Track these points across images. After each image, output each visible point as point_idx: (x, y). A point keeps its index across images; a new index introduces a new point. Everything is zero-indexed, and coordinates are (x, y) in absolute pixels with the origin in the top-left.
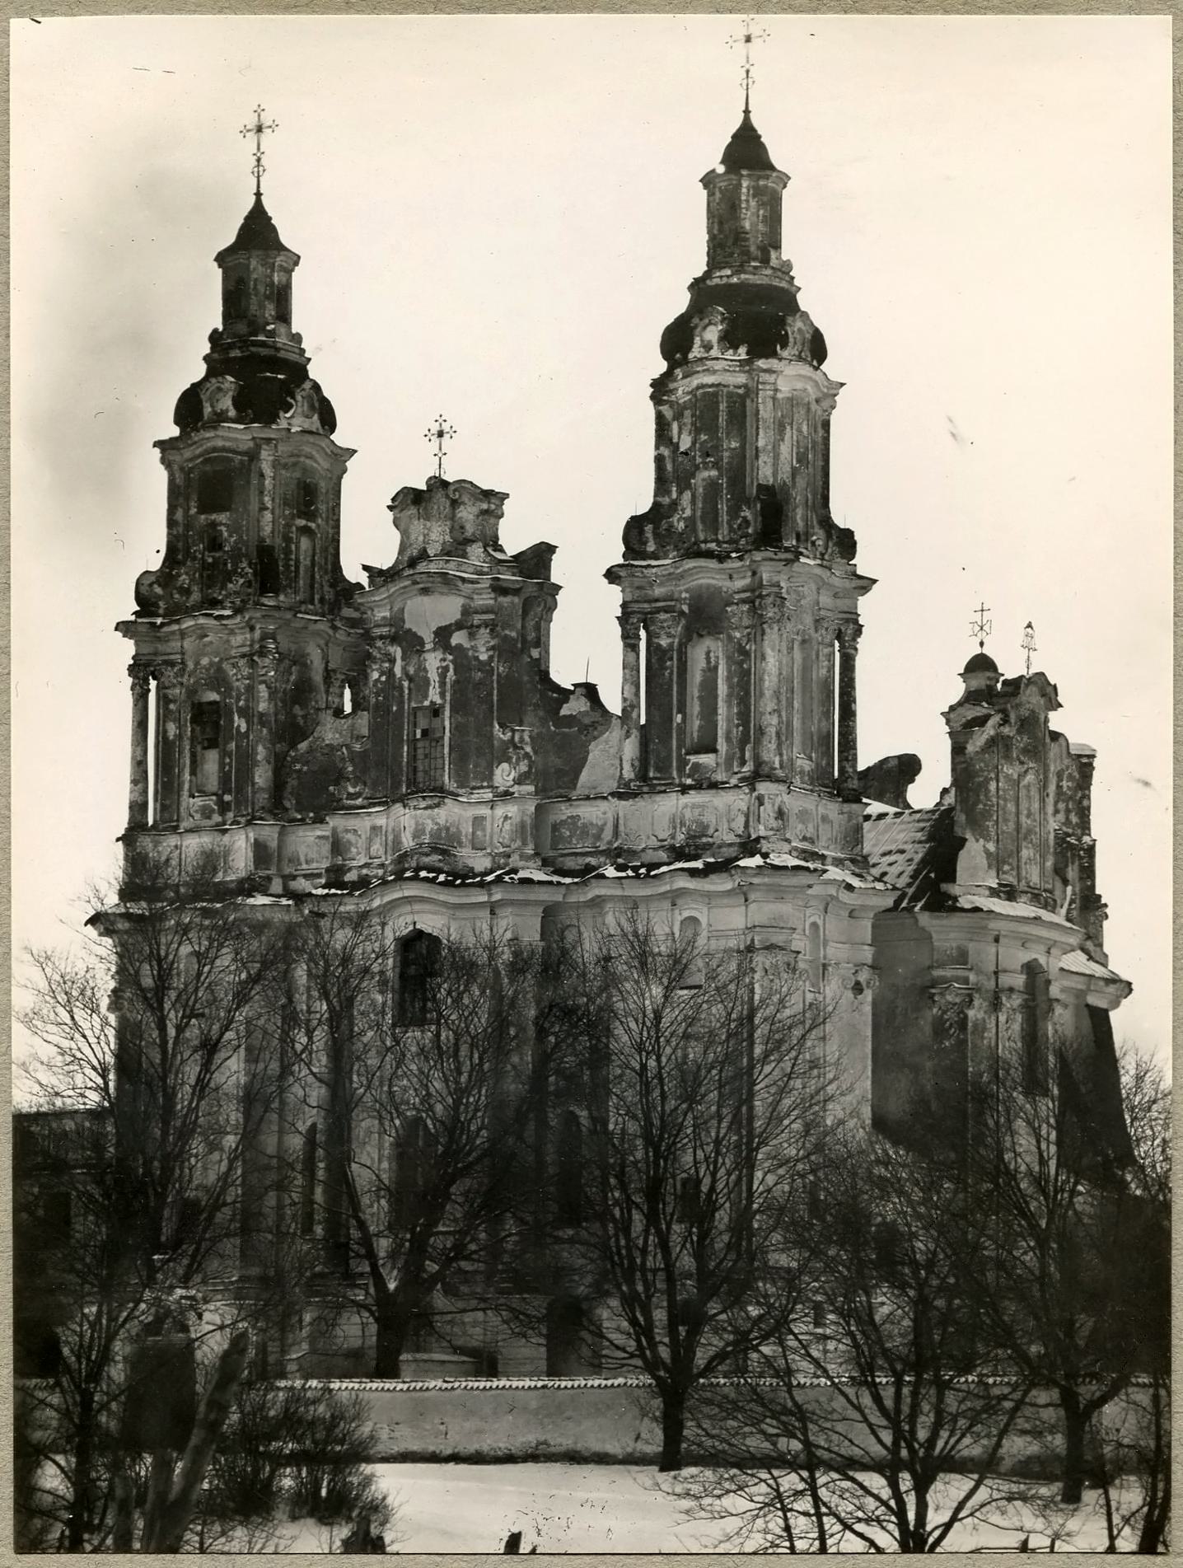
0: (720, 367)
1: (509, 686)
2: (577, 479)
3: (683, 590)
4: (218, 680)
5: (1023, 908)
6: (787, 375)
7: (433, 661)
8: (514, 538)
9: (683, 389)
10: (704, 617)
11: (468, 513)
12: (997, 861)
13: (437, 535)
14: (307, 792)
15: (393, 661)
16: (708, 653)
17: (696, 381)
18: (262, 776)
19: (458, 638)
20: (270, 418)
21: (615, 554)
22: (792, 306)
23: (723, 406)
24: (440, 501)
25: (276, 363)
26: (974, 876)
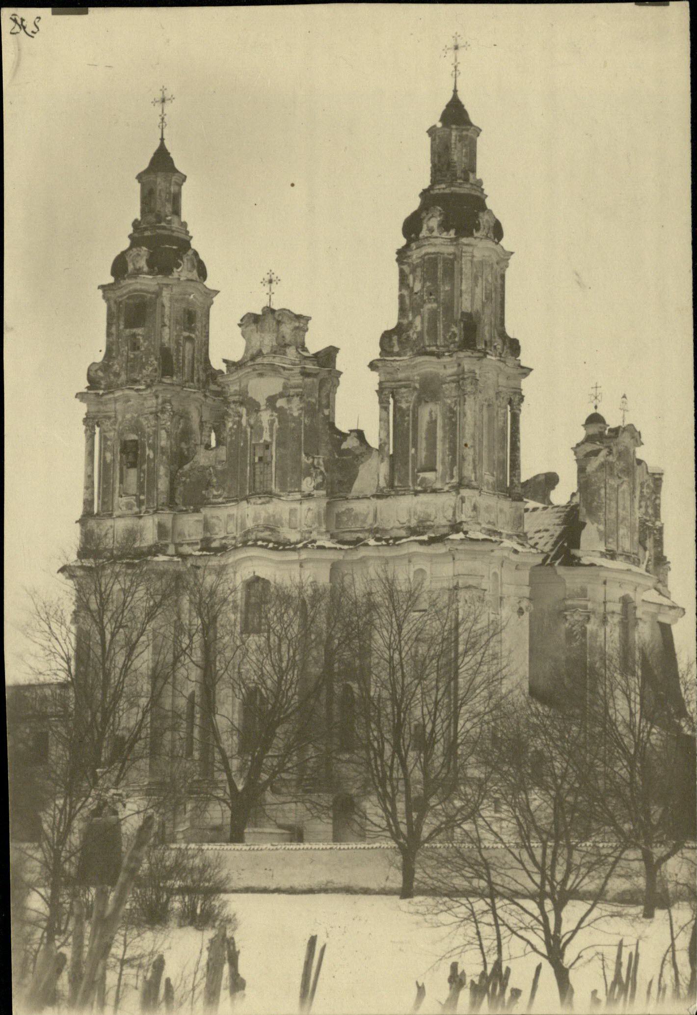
0: (438, 242)
1: (311, 431)
2: (352, 309)
3: (415, 375)
4: (137, 428)
5: (619, 564)
6: (478, 247)
7: (265, 417)
8: (315, 343)
9: (415, 255)
11: (287, 329)
12: (605, 536)
13: (267, 341)
15: (241, 416)
17: (424, 251)
18: (163, 484)
19: (281, 403)
21: (375, 353)
22: (483, 207)
23: (440, 266)
24: (270, 322)
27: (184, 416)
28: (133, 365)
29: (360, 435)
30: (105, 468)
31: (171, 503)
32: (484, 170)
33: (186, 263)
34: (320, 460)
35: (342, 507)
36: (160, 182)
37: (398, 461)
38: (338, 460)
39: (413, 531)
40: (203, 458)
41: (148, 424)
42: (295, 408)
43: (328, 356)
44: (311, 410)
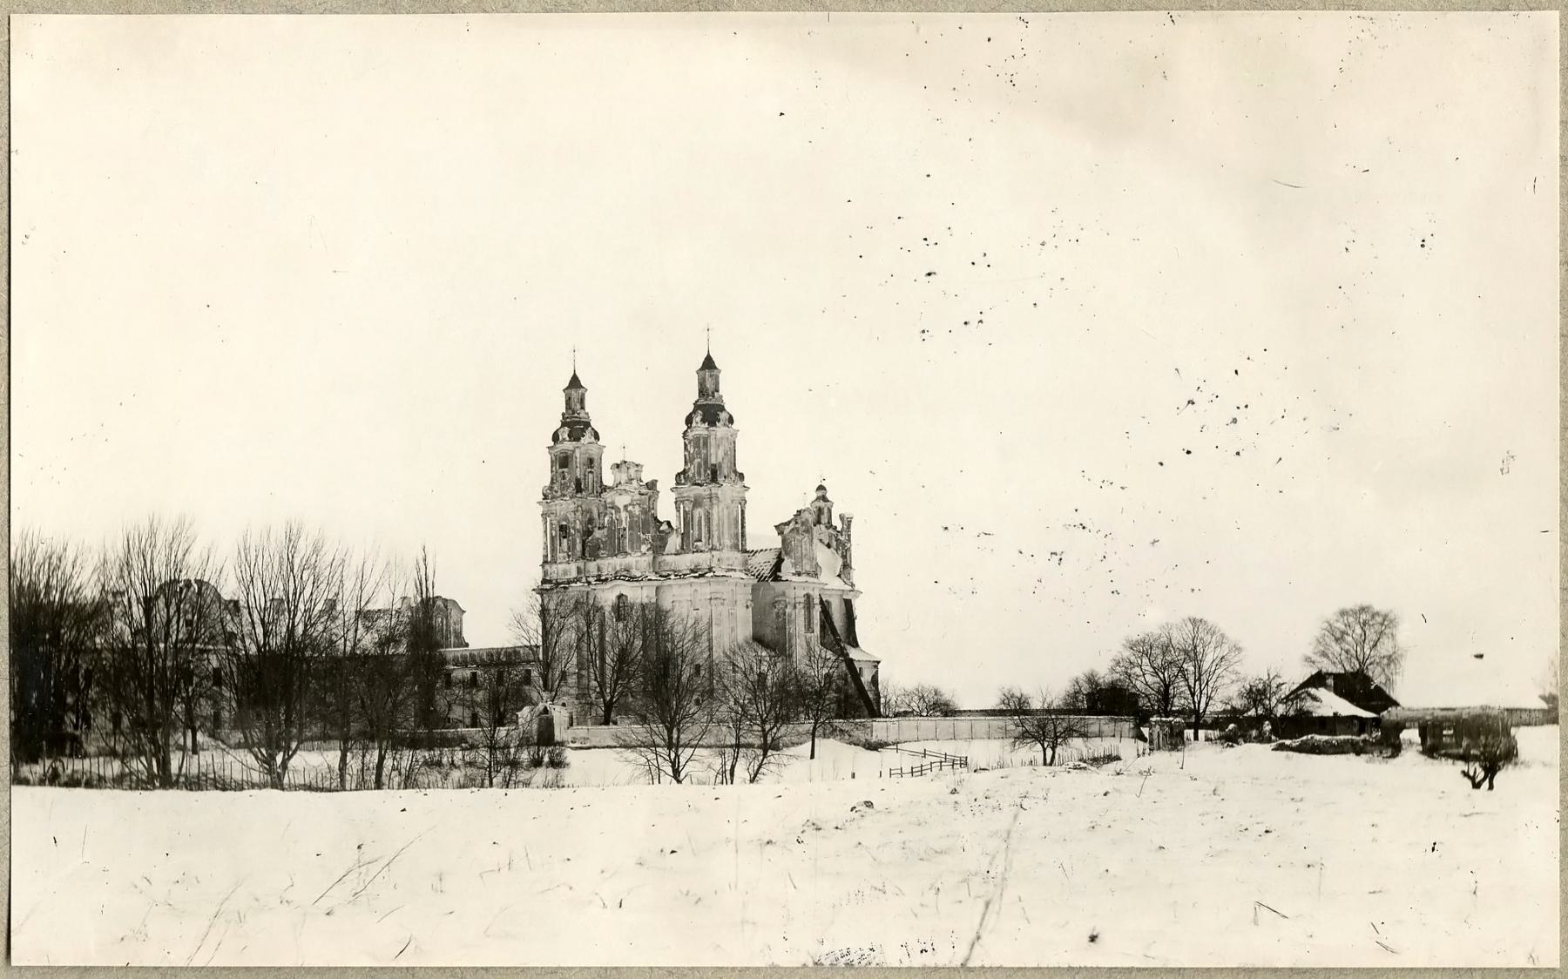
0: (700, 429)
1: (645, 522)
2: (662, 459)
4: (566, 519)
5: (803, 578)
6: (720, 430)
7: (624, 515)
8: (647, 478)
9: (691, 435)
10: (697, 503)
11: (632, 471)
12: (795, 565)
13: (624, 478)
14: (590, 551)
16: (699, 512)
18: (579, 547)
20: (578, 439)
21: (673, 484)
22: (722, 409)
24: (624, 468)
25: (579, 423)
26: (787, 569)
27: (589, 511)
28: (564, 487)
29: (669, 523)
30: (552, 538)
31: (583, 556)
32: (724, 390)
33: (588, 433)
34: (649, 536)
35: (660, 558)
36: (574, 394)
37: (685, 536)
38: (657, 534)
39: (692, 571)
40: (597, 534)
41: (571, 517)
42: (637, 511)
43: (652, 485)
44: (645, 512)
